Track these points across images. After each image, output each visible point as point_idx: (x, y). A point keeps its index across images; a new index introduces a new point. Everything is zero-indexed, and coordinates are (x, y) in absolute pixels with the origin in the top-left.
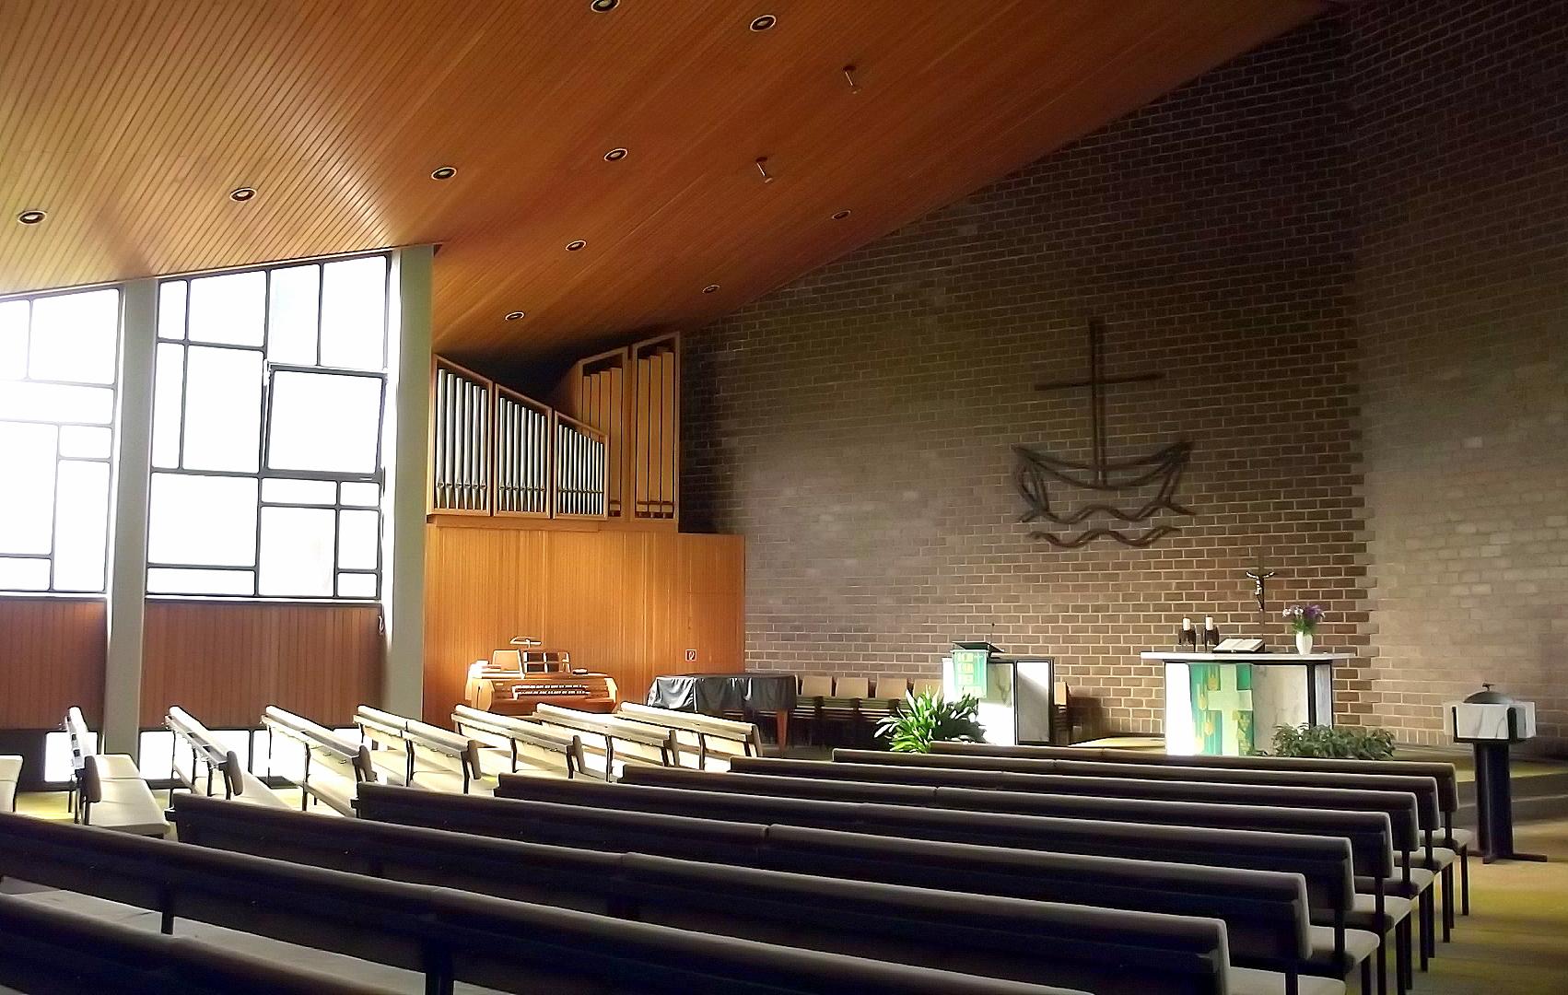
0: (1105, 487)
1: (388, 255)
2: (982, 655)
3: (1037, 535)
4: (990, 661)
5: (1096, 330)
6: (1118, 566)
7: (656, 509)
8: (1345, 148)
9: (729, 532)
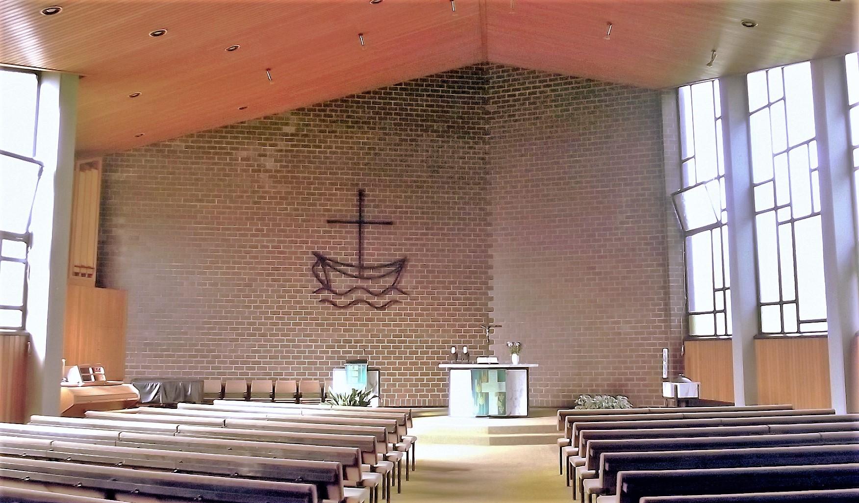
0: (361, 277)
1: (40, 75)
2: (363, 367)
3: (323, 301)
5: (361, 194)
7: (84, 271)
9: (112, 287)
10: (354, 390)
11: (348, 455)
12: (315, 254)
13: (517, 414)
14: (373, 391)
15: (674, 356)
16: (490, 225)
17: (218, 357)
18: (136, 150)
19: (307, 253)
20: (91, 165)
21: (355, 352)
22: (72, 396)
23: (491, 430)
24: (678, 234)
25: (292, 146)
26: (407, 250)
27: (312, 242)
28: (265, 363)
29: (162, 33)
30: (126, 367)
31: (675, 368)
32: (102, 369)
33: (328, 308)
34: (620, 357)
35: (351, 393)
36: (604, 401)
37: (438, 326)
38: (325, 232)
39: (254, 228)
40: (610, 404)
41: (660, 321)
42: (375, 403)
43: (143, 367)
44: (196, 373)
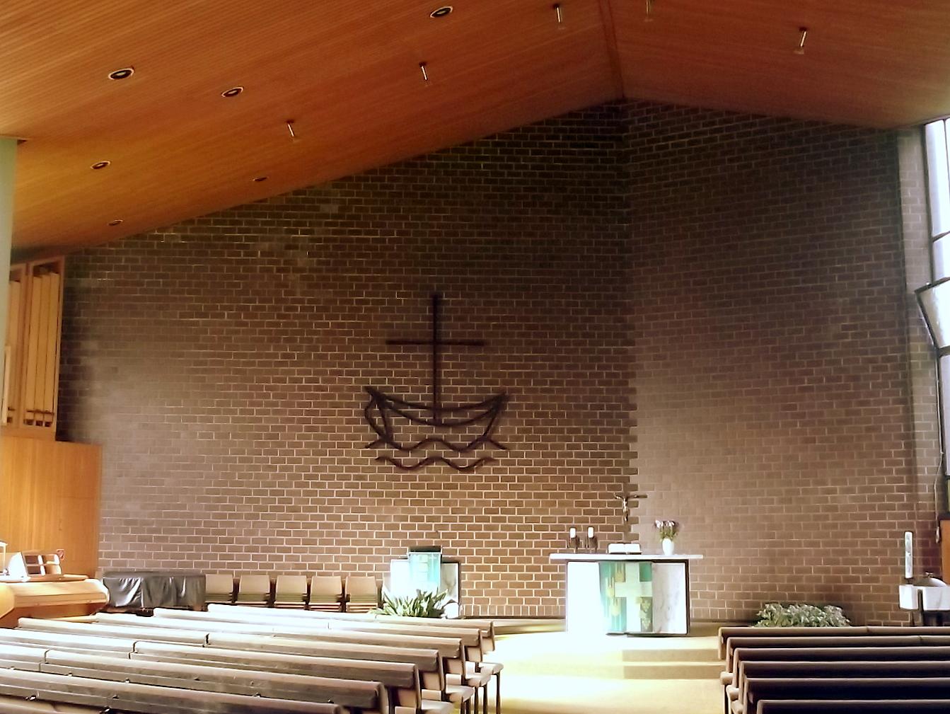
0: (437, 423)
2: (435, 557)
3: (381, 459)
4: (443, 562)
5: (436, 302)
6: (448, 487)
7: (39, 417)
8: (621, 198)
9: (81, 441)
10: (419, 591)
11: (365, 693)
12: (367, 389)
13: (670, 632)
14: (450, 593)
15: (924, 544)
16: (632, 343)
17: (230, 541)
18: (112, 245)
19: (357, 389)
20: (52, 268)
21: (429, 535)
22: (11, 596)
23: (628, 656)
24: (928, 353)
25: (335, 232)
26: (504, 383)
27: (365, 373)
28: (296, 550)
29: (128, 73)
30: (100, 555)
31: (925, 562)
32: (56, 557)
33: (389, 470)
34: (836, 544)
35: (415, 596)
36: (804, 612)
37: (553, 496)
38: (382, 357)
39: (280, 353)
40: (813, 618)
41: (900, 489)
42: (452, 611)
43: (124, 555)
44: (181, 565)
